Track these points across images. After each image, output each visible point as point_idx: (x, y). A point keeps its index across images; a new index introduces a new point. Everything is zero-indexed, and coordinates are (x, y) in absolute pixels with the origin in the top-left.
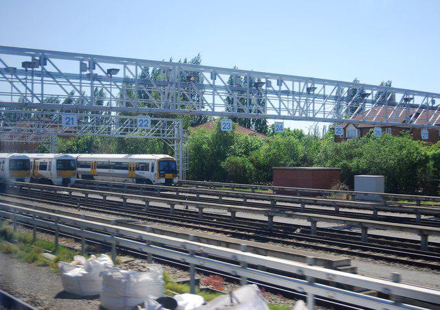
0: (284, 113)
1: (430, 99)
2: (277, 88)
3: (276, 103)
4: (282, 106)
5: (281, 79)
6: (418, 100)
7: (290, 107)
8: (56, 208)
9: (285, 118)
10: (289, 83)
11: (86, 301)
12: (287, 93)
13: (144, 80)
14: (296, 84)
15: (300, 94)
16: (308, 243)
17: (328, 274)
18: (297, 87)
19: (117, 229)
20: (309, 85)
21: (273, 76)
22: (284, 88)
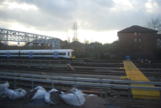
0: (20, 40)
1: (32, 35)
2: (18, 34)
3: (10, 37)
4: (12, 38)
5: (19, 32)
6: (51, 38)
7: (21, 39)
8: (11, 74)
9: (20, 41)
10: (20, 33)
11: (147, 95)
12: (20, 36)
13: (52, 39)
14: (22, 34)
15: (23, 36)
16: (103, 73)
17: (18, 74)
18: (22, 34)
19: (59, 78)
20: (25, 34)
21: (17, 32)
22: (19, 34)
